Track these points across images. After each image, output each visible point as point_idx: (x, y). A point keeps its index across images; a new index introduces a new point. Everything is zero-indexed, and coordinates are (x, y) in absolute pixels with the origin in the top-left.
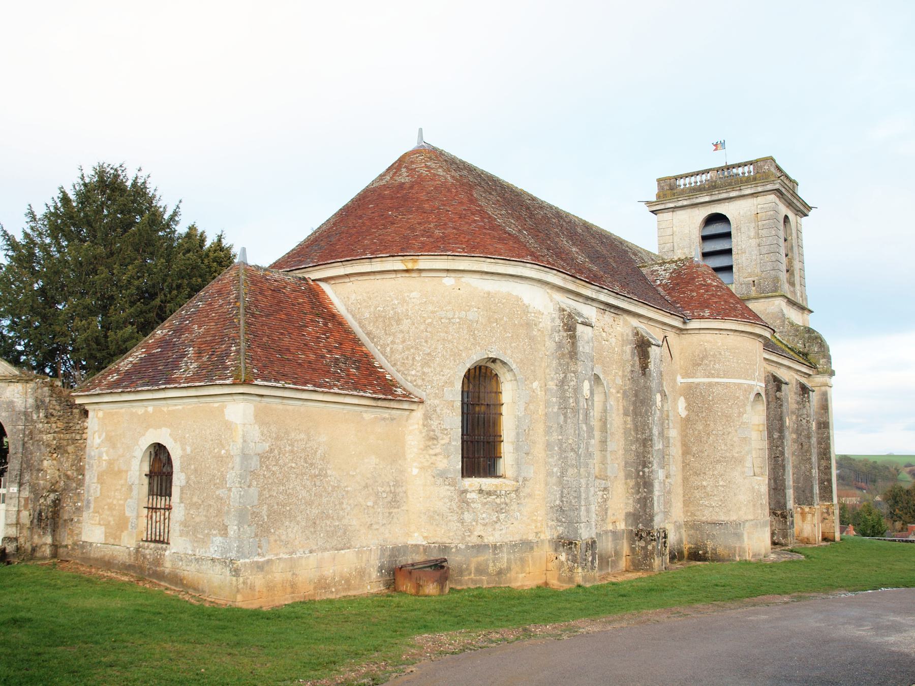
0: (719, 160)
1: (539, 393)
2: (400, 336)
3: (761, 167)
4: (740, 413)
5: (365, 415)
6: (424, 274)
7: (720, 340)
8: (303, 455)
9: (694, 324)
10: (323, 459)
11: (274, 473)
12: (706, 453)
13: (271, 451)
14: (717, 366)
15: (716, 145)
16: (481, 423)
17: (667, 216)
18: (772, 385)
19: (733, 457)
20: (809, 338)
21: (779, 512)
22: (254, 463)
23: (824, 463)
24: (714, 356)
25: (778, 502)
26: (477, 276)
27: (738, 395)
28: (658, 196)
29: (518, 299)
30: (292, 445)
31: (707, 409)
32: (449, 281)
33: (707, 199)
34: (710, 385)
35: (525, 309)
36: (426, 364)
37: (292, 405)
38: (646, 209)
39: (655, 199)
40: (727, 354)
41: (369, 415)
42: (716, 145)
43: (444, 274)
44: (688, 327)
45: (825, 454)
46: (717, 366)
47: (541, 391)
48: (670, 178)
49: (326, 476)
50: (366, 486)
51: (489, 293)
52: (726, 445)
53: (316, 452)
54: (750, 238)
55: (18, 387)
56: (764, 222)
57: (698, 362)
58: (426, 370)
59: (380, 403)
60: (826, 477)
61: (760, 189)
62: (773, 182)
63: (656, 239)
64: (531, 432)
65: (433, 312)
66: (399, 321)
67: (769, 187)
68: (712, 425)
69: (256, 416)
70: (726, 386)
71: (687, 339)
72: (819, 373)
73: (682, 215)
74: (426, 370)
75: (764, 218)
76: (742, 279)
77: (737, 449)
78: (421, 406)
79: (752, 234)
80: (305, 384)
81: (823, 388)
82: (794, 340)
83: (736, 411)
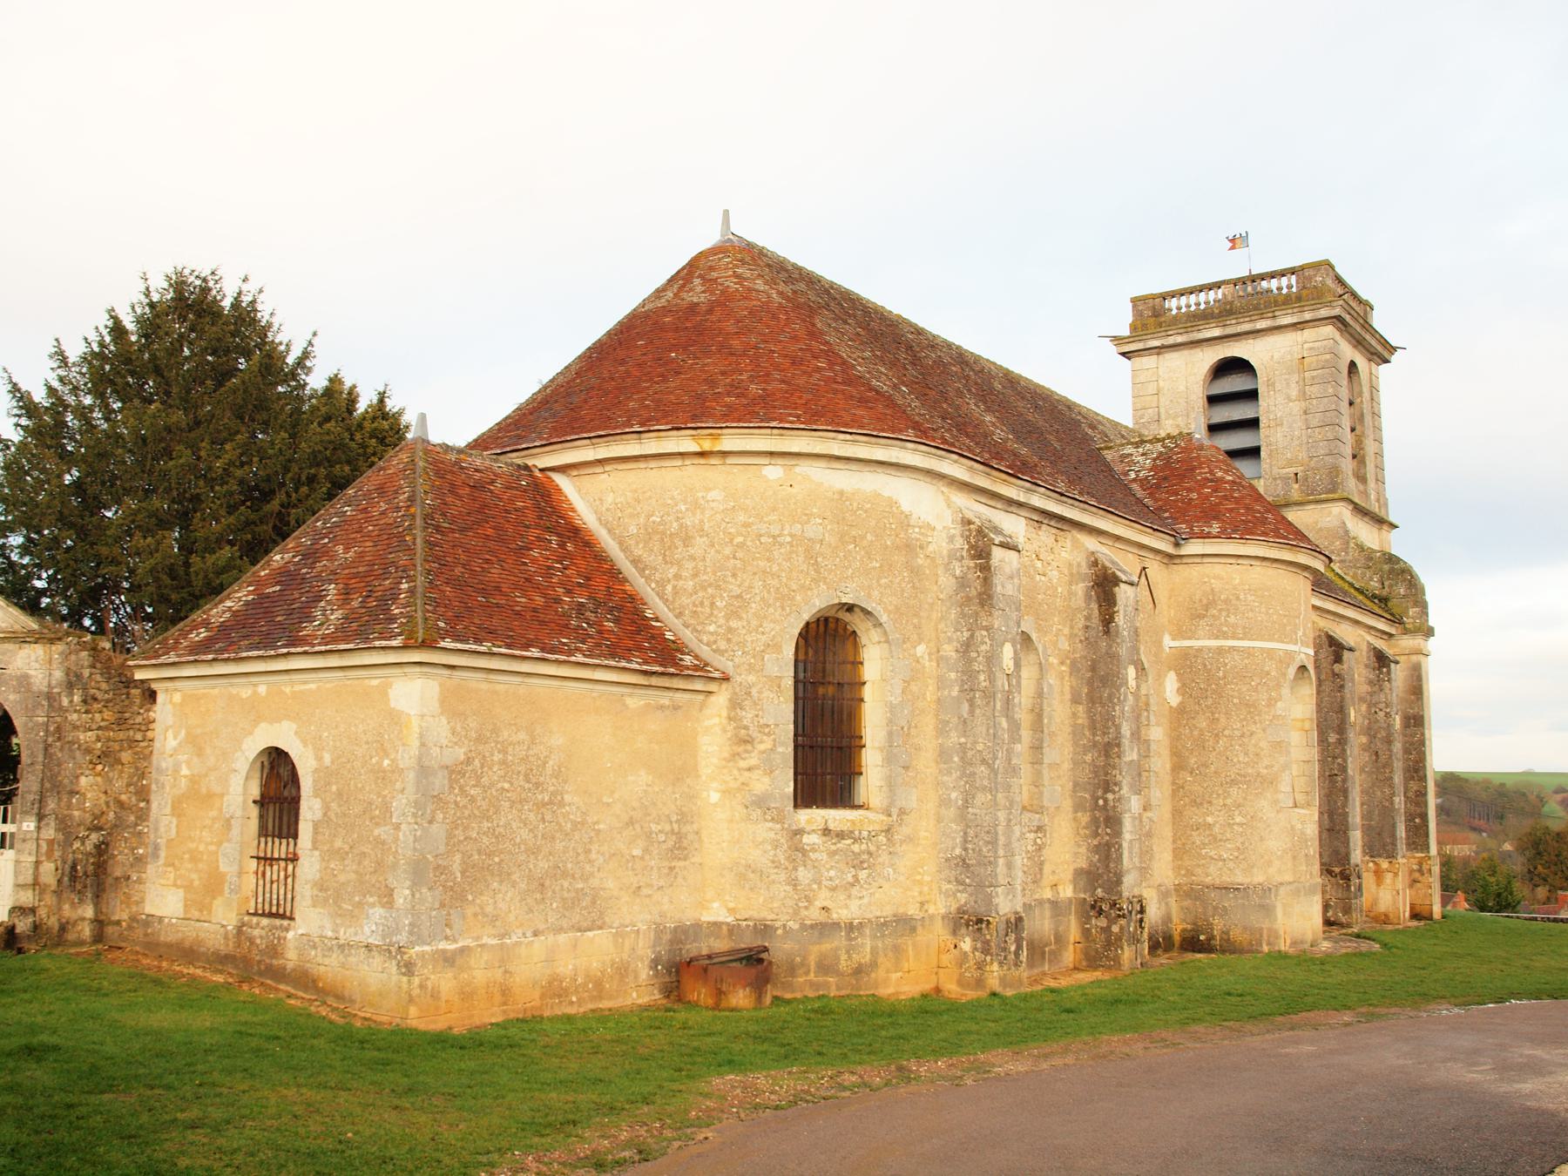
1: (927, 664)
2: (690, 565)
3: (1310, 278)
4: (1270, 699)
6: (730, 460)
8: (522, 768)
9: (1194, 547)
10: (557, 774)
11: (473, 800)
13: (469, 761)
14: (1232, 619)
15: (1233, 241)
17: (1148, 361)
20: (1391, 571)
22: (439, 782)
23: (1414, 786)
24: (1227, 601)
25: (1336, 852)
26: (822, 463)
27: (1267, 668)
28: (1133, 327)
29: (892, 503)
30: (504, 752)
31: (1214, 691)
32: (774, 472)
33: (1217, 332)
34: (1220, 650)
35: (905, 521)
36: (733, 614)
38: (1112, 350)
39: (1127, 333)
41: (635, 701)
42: (1233, 241)
44: (1183, 551)
45: (1416, 771)
46: (1232, 619)
48: (1154, 297)
49: (562, 804)
50: (631, 822)
51: (841, 493)
52: (1246, 754)
53: (545, 763)
54: (1291, 401)
55: (38, 651)
56: (1315, 373)
57: (1201, 611)
58: (734, 624)
59: (654, 681)
61: (1307, 316)
63: (1130, 399)
65: (746, 525)
67: (1324, 313)
68: (1223, 719)
70: (1248, 652)
71: (1181, 572)
72: (1406, 632)
73: (1174, 360)
74: (734, 624)
75: (1314, 366)
76: (1275, 471)
77: (1266, 762)
78: (725, 685)
79: (1294, 393)
80: (526, 647)
81: (1414, 658)
82: (1364, 575)
83: (1265, 696)
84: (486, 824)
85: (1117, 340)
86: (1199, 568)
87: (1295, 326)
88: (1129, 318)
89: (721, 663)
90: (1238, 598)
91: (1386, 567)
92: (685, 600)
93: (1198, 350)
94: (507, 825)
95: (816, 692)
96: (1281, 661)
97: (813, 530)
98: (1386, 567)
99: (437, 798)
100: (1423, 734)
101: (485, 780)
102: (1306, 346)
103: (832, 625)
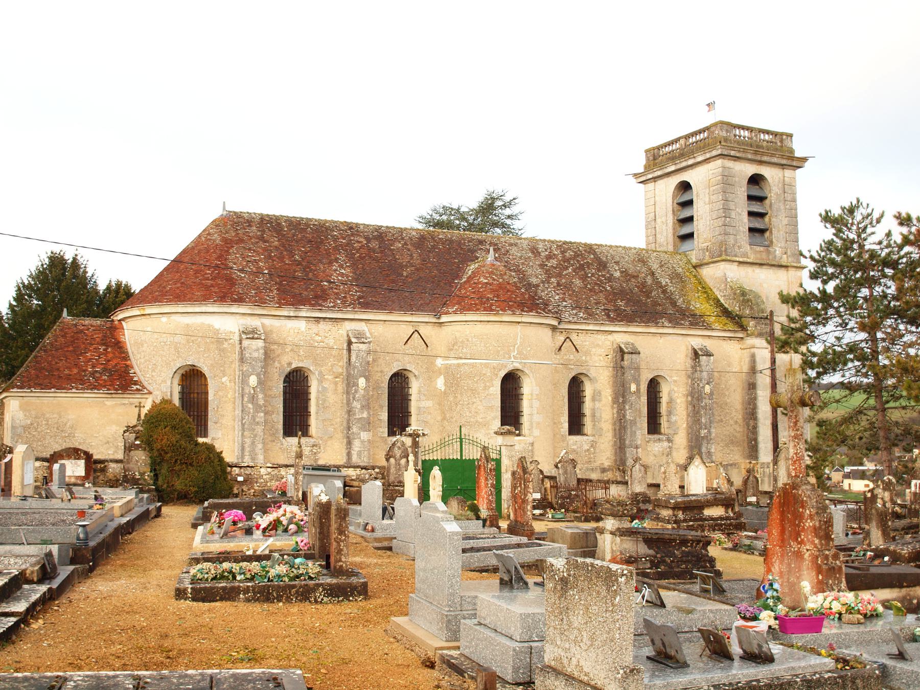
0: (707, 120)
1: (228, 384)
2: (143, 354)
3: (713, 132)
4: (485, 386)
5: (107, 403)
6: (152, 316)
7: (467, 330)
8: (56, 426)
9: (444, 319)
10: (72, 427)
11: (34, 436)
12: (454, 419)
13: (32, 424)
14: (465, 350)
15: (708, 105)
16: (196, 405)
17: (651, 186)
18: (619, 354)
19: (477, 422)
20: (743, 300)
21: (621, 468)
22: (20, 430)
23: (752, 423)
24: (462, 342)
25: (621, 459)
26: (180, 315)
27: (484, 372)
28: (645, 167)
29: (209, 326)
31: (456, 384)
32: (164, 319)
33: (673, 168)
34: (459, 365)
35: (217, 332)
36: (153, 371)
37: (46, 400)
39: (642, 170)
40: (474, 340)
41: (109, 402)
42: (708, 105)
43: (161, 316)
44: (441, 321)
45: (753, 415)
46: (465, 350)
47: (230, 382)
48: (654, 149)
49: (74, 437)
50: (108, 442)
51: (188, 325)
52: (470, 412)
53: (65, 425)
54: (706, 204)
56: (714, 188)
58: (153, 374)
59: (114, 396)
60: (754, 437)
61: (708, 156)
62: (714, 148)
63: (644, 208)
64: (219, 410)
65: (157, 339)
66: (142, 345)
67: (714, 153)
68: (459, 396)
69: (20, 407)
70: (473, 365)
72: (748, 335)
74: (153, 374)
75: (714, 184)
77: (482, 416)
78: (151, 395)
79: (707, 200)
80: (50, 389)
81: (752, 350)
82: (733, 303)
83: (482, 385)
84: (40, 443)
85: (636, 175)
86: (451, 327)
87: (706, 161)
88: (643, 161)
89: (150, 388)
90: (468, 340)
91: (741, 298)
92: (142, 366)
93: (670, 178)
94: (49, 443)
95: (190, 396)
96: (494, 368)
97: (178, 339)
98: (741, 298)
99: (19, 435)
100: (755, 394)
101: (39, 430)
102: (711, 172)
103: (195, 372)
